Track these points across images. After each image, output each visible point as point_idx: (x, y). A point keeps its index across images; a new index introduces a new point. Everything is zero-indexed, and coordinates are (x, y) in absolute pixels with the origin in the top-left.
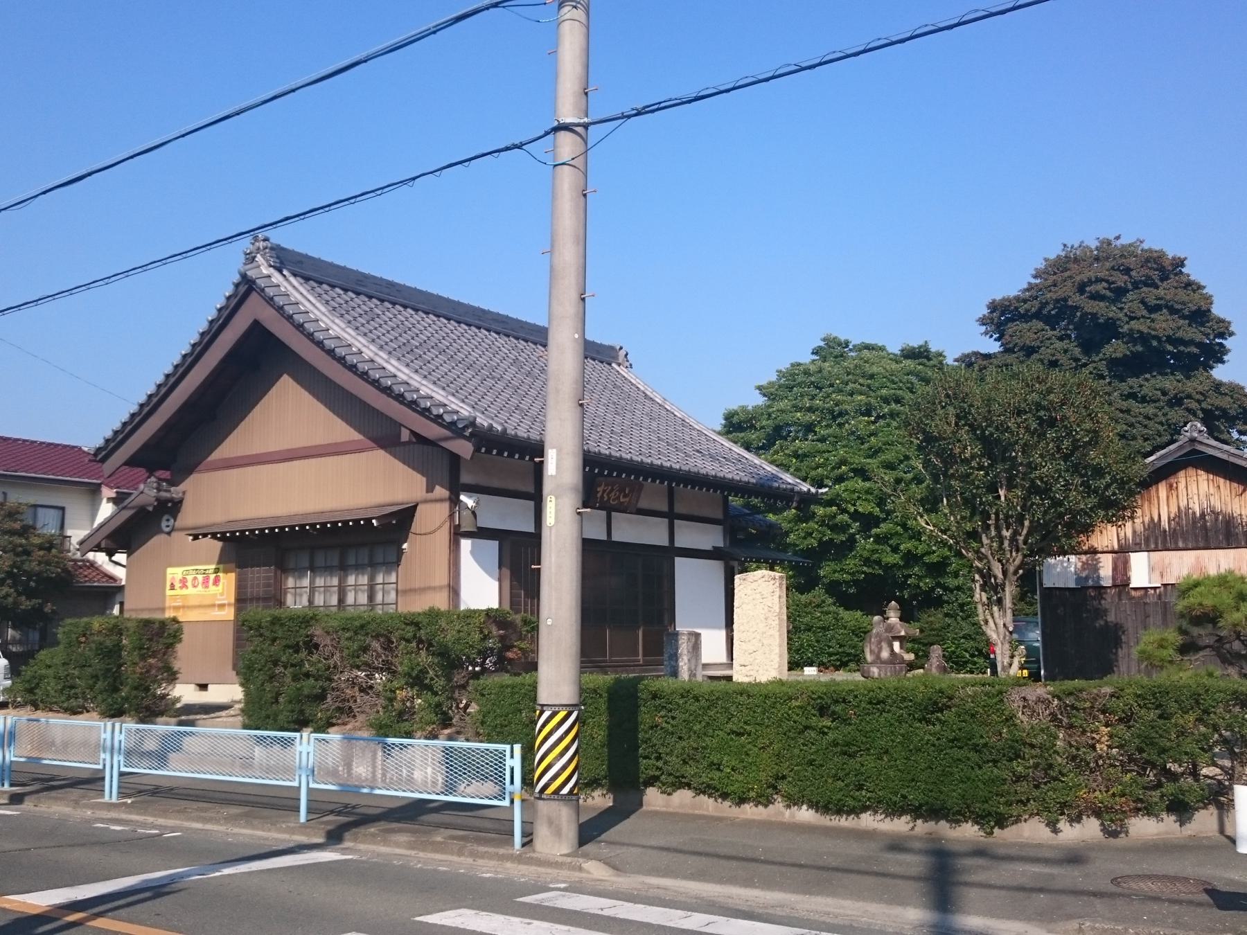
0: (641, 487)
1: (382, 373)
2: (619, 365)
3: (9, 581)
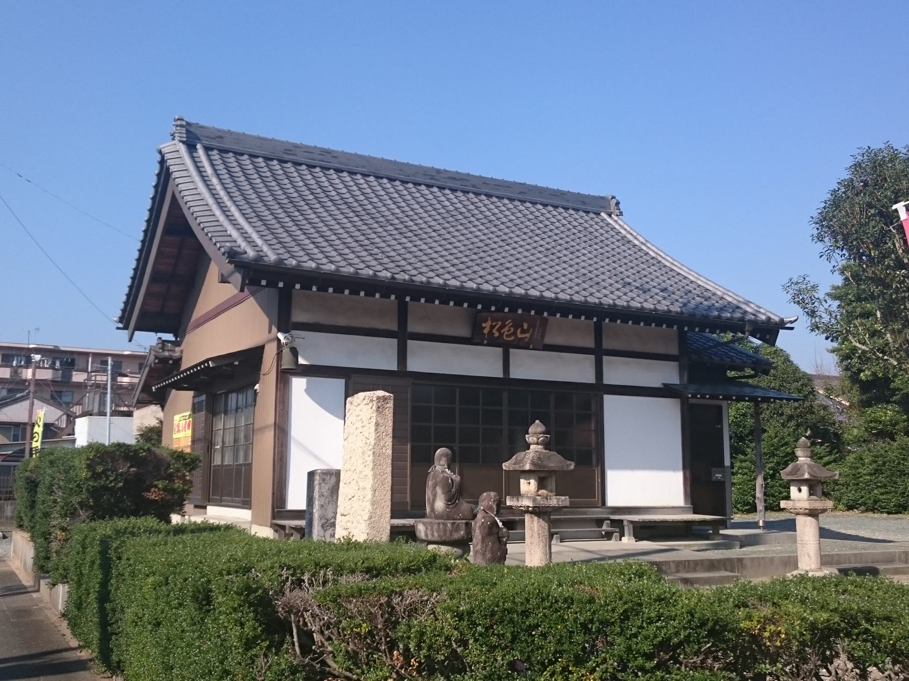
0: (545, 322)
1: (694, 286)
2: (610, 215)
3: (750, 422)
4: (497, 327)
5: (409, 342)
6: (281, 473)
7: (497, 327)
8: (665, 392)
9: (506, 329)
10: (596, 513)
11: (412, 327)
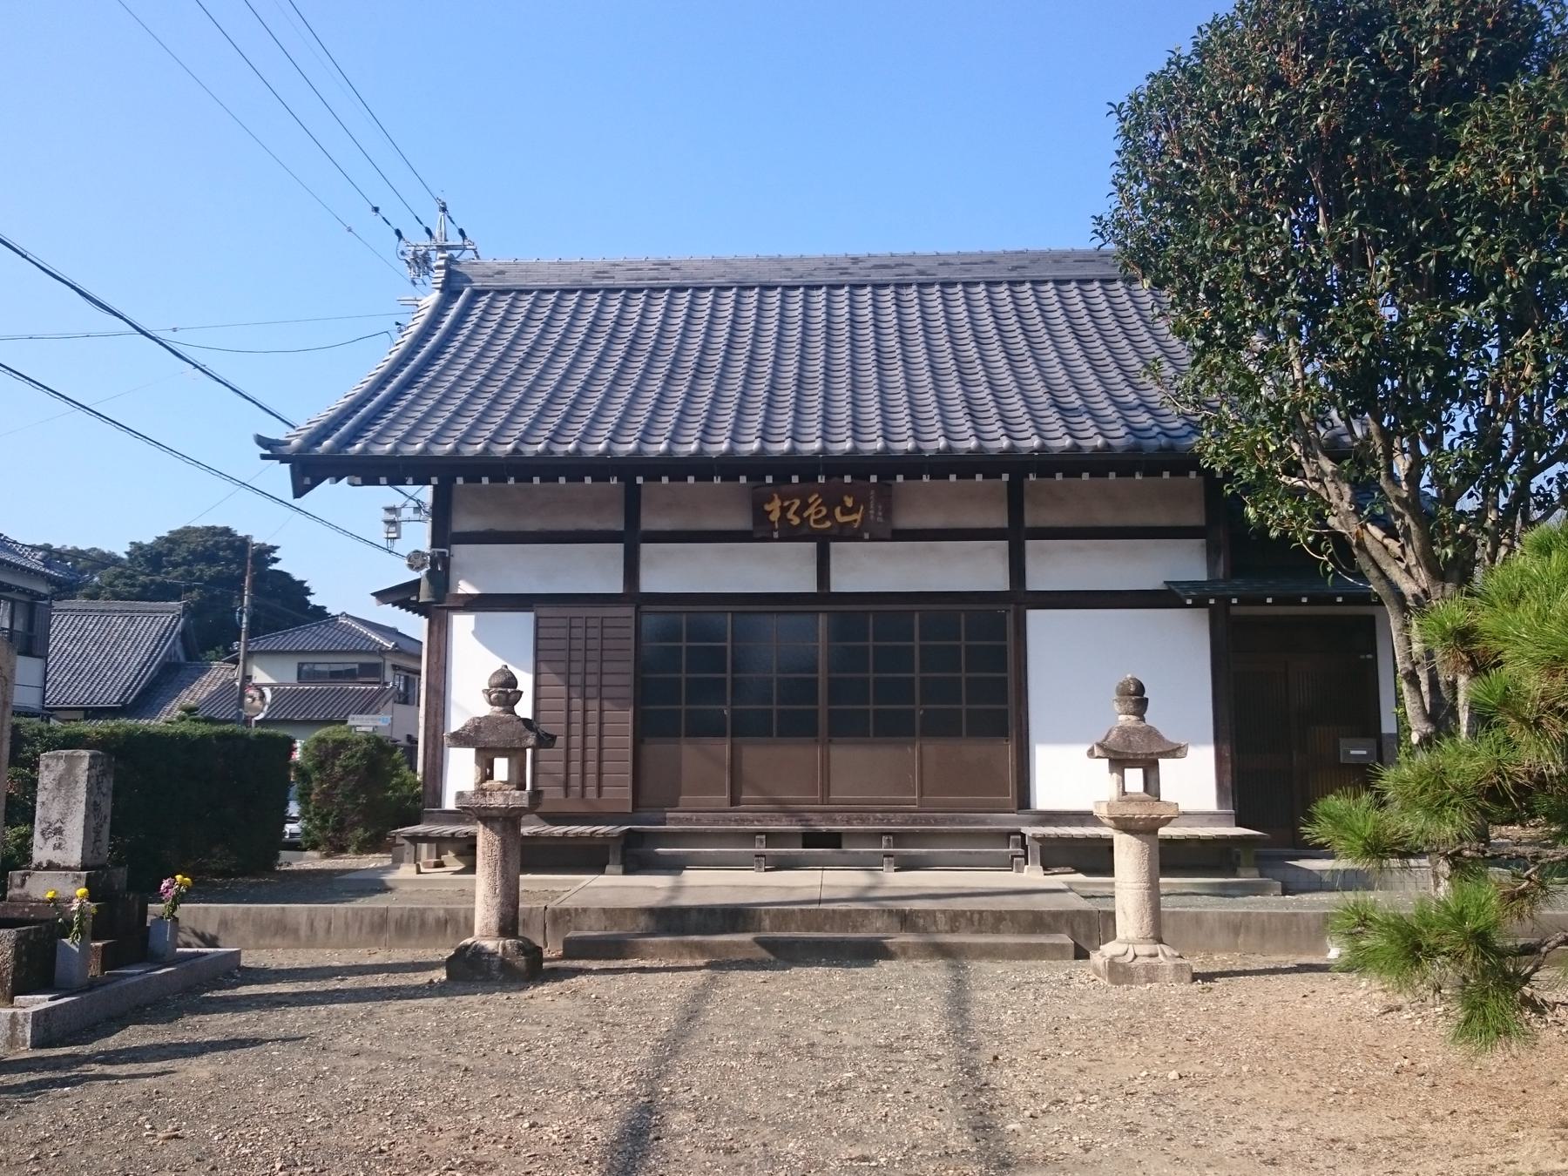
4: (794, 508)
5: (1029, 544)
6: (434, 756)
7: (794, 508)
8: (1165, 598)
9: (812, 510)
10: (1007, 821)
11: (649, 522)
